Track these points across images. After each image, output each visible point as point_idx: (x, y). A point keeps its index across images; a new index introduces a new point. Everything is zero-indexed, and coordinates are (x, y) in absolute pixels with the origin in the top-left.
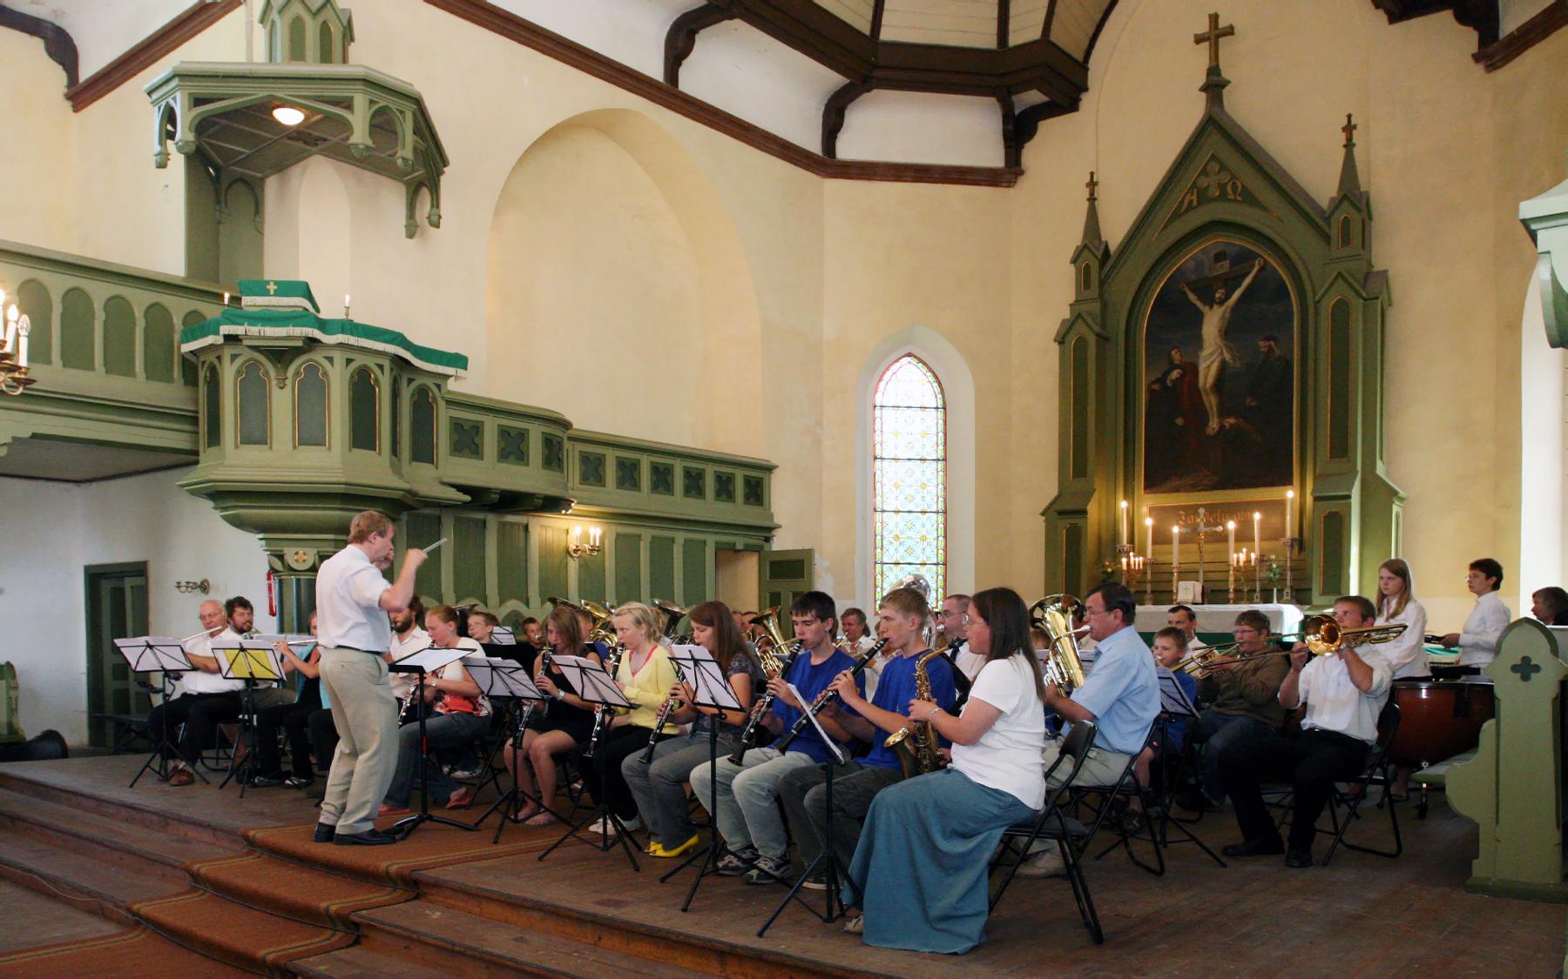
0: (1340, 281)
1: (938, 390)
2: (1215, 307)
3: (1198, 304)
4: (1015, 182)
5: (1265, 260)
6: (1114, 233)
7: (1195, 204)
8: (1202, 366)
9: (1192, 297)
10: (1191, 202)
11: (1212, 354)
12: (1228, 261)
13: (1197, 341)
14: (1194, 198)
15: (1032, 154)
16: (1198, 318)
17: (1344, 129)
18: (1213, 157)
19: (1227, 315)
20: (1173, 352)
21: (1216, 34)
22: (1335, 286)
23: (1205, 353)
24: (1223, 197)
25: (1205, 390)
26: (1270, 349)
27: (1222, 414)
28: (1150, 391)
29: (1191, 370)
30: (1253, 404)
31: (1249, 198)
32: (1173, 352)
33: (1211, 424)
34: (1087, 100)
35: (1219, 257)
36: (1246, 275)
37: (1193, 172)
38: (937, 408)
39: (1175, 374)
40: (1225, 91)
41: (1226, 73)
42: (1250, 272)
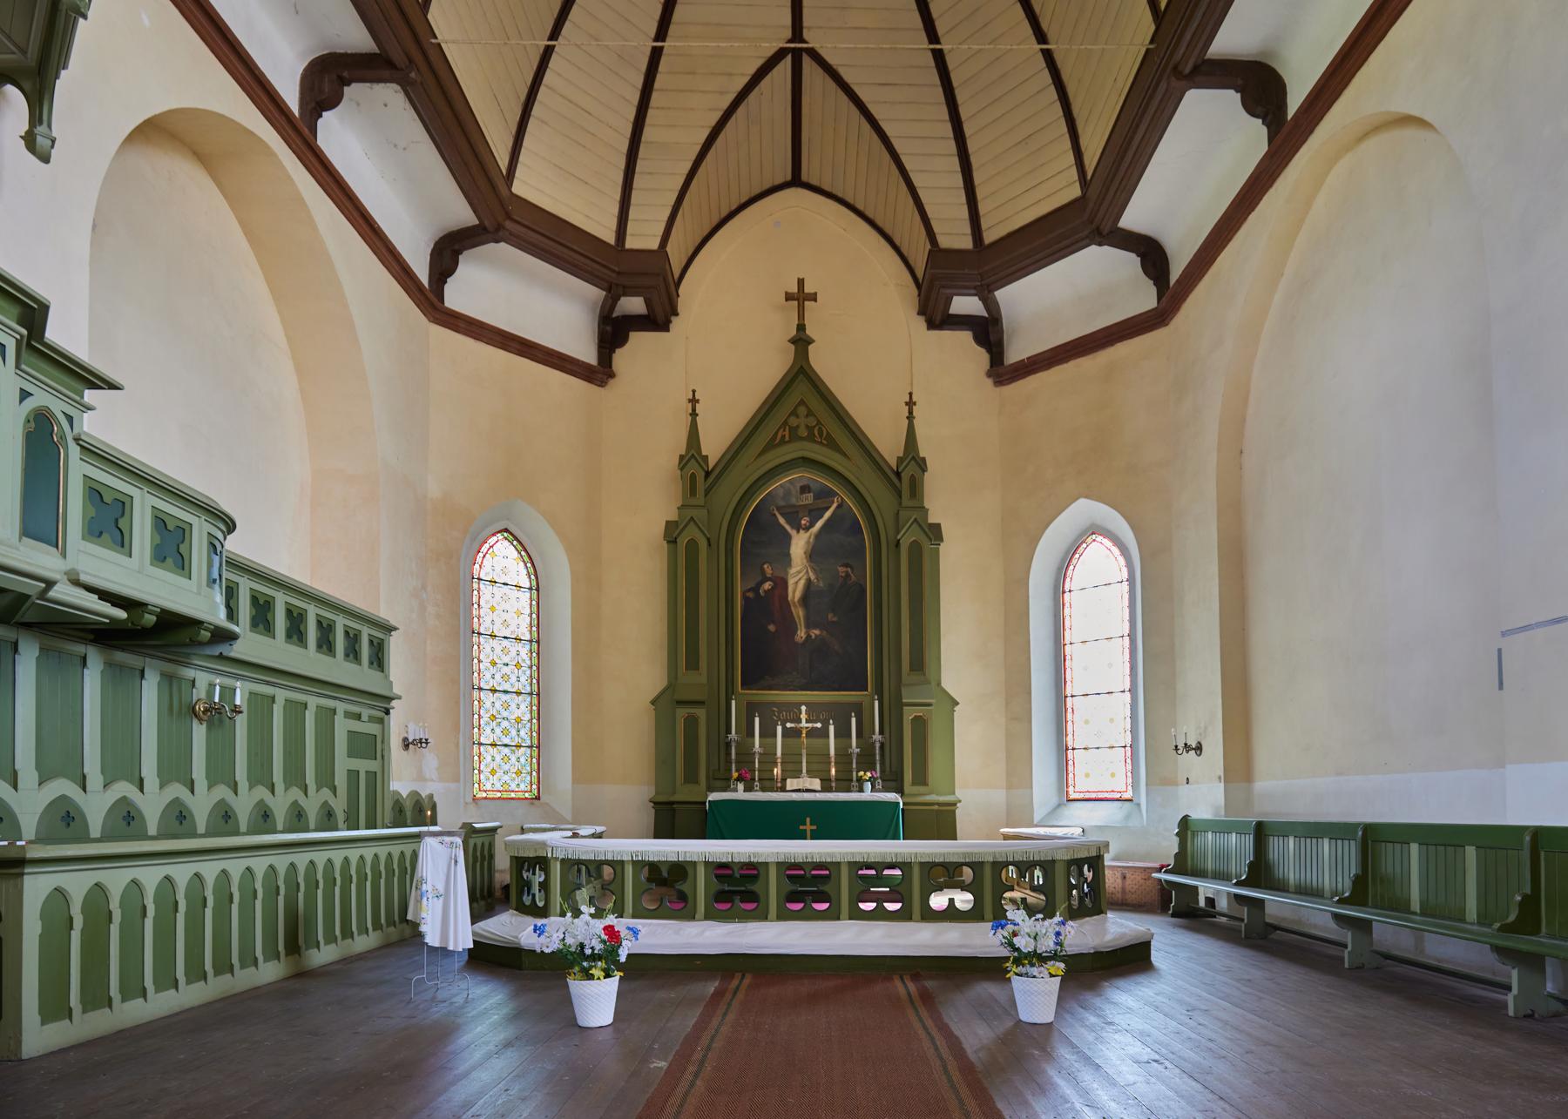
0: (915, 525)
3: (788, 527)
6: (714, 446)
7: (787, 438)
8: (791, 582)
9: (782, 521)
10: (784, 436)
11: (799, 572)
12: (812, 494)
13: (786, 558)
14: (787, 433)
15: (621, 358)
18: (802, 402)
19: (811, 540)
20: (765, 566)
21: (801, 297)
23: (793, 571)
24: (810, 438)
25: (794, 603)
26: (848, 575)
27: (808, 626)
28: (745, 599)
29: (782, 584)
30: (835, 619)
31: (832, 444)
32: (765, 566)
33: (799, 632)
35: (805, 489)
39: (767, 586)
41: (810, 331)
42: (830, 507)
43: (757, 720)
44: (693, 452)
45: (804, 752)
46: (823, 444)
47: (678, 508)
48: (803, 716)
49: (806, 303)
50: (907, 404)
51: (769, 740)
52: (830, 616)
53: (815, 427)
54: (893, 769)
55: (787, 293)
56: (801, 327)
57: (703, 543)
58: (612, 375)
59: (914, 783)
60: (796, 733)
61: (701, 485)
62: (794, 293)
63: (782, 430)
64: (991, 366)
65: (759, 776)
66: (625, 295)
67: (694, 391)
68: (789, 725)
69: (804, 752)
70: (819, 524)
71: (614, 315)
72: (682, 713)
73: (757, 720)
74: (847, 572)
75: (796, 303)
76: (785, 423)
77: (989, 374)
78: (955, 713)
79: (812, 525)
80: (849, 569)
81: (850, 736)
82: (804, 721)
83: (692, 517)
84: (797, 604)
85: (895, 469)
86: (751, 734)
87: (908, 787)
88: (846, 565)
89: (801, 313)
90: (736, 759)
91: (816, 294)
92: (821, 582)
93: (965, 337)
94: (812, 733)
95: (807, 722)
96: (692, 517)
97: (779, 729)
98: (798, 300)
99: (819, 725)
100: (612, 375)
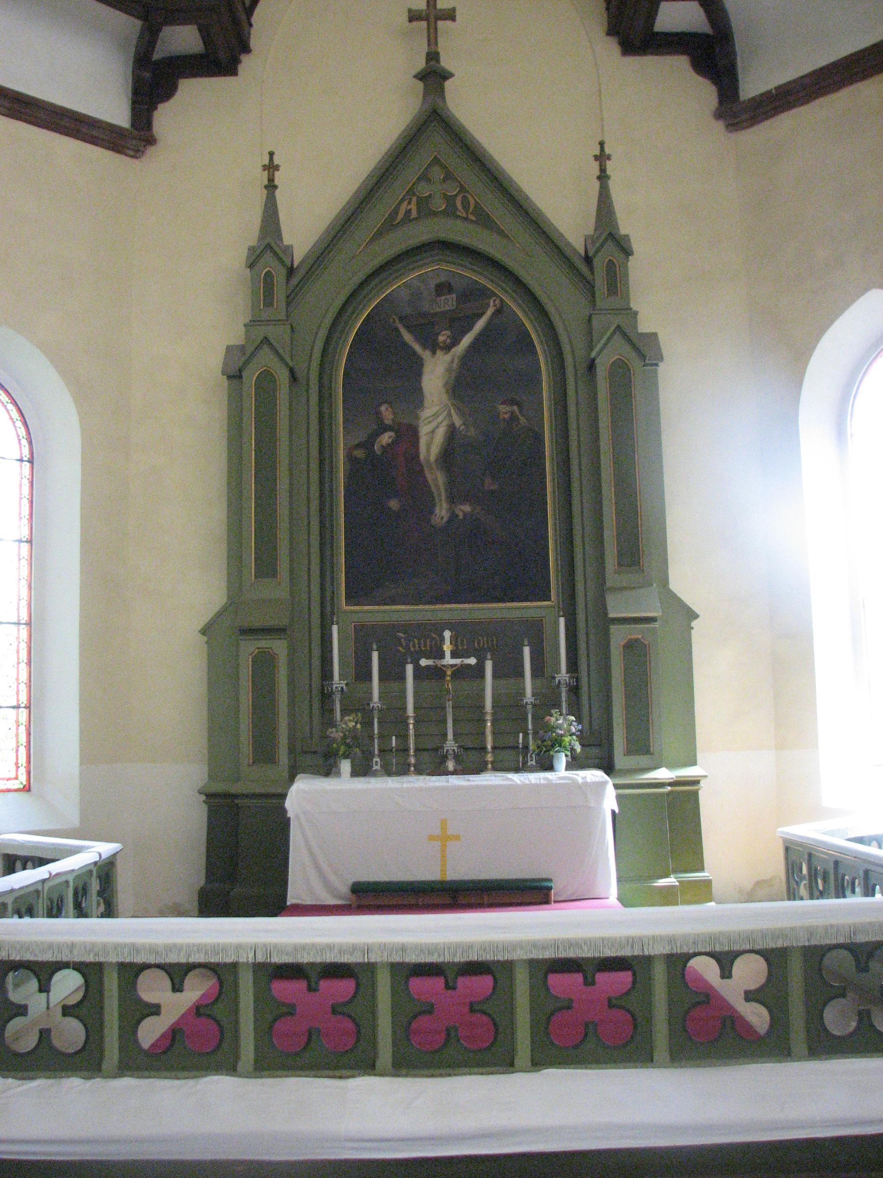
0: (618, 336)
1: (22, 431)
2: (439, 353)
3: (417, 348)
4: (143, 152)
5: (502, 300)
7: (414, 214)
8: (424, 430)
9: (407, 337)
10: (408, 212)
11: (436, 415)
12: (454, 296)
14: (413, 207)
16: (416, 368)
17: (265, 168)
18: (436, 161)
19: (455, 365)
20: (383, 408)
22: (612, 342)
23: (426, 413)
24: (450, 212)
25: (428, 461)
26: (513, 418)
27: (452, 500)
28: (351, 459)
30: (494, 487)
31: (484, 220)
32: (383, 408)
33: (437, 511)
34: (247, 63)
35: (443, 288)
36: (480, 316)
37: (410, 173)
38: (21, 460)
39: (386, 438)
40: (448, 84)
42: (482, 314)
43: (375, 655)
44: (269, 240)
45: (449, 705)
46: (472, 221)
47: (245, 325)
48: (447, 648)
49: (440, 24)
50: (596, 158)
51: (395, 686)
52: (487, 481)
53: (456, 196)
54: (596, 727)
55: (410, 11)
56: (433, 56)
57: (283, 376)
58: (151, 141)
59: (629, 752)
60: (437, 673)
61: (280, 292)
62: (422, 11)
63: (406, 203)
64: (721, 103)
65: (379, 746)
66: (172, 23)
67: (271, 154)
68: (424, 662)
69: (449, 705)
70: (467, 340)
71: (156, 57)
72: (249, 647)
73: (375, 655)
74: (512, 413)
75: (424, 24)
76: (411, 192)
77: (719, 115)
78: (693, 631)
79: (455, 342)
80: (515, 408)
81: (521, 675)
82: (448, 654)
83: (266, 338)
84: (434, 466)
85: (583, 254)
86: (367, 676)
87: (620, 760)
88: (513, 402)
89: (432, 36)
90: (379, 733)
91: (454, 10)
92: (472, 429)
93: (680, 64)
94: (460, 672)
95: (454, 655)
96: (266, 338)
97: (410, 668)
98: (427, 19)
99: (472, 661)
100: (151, 141)
